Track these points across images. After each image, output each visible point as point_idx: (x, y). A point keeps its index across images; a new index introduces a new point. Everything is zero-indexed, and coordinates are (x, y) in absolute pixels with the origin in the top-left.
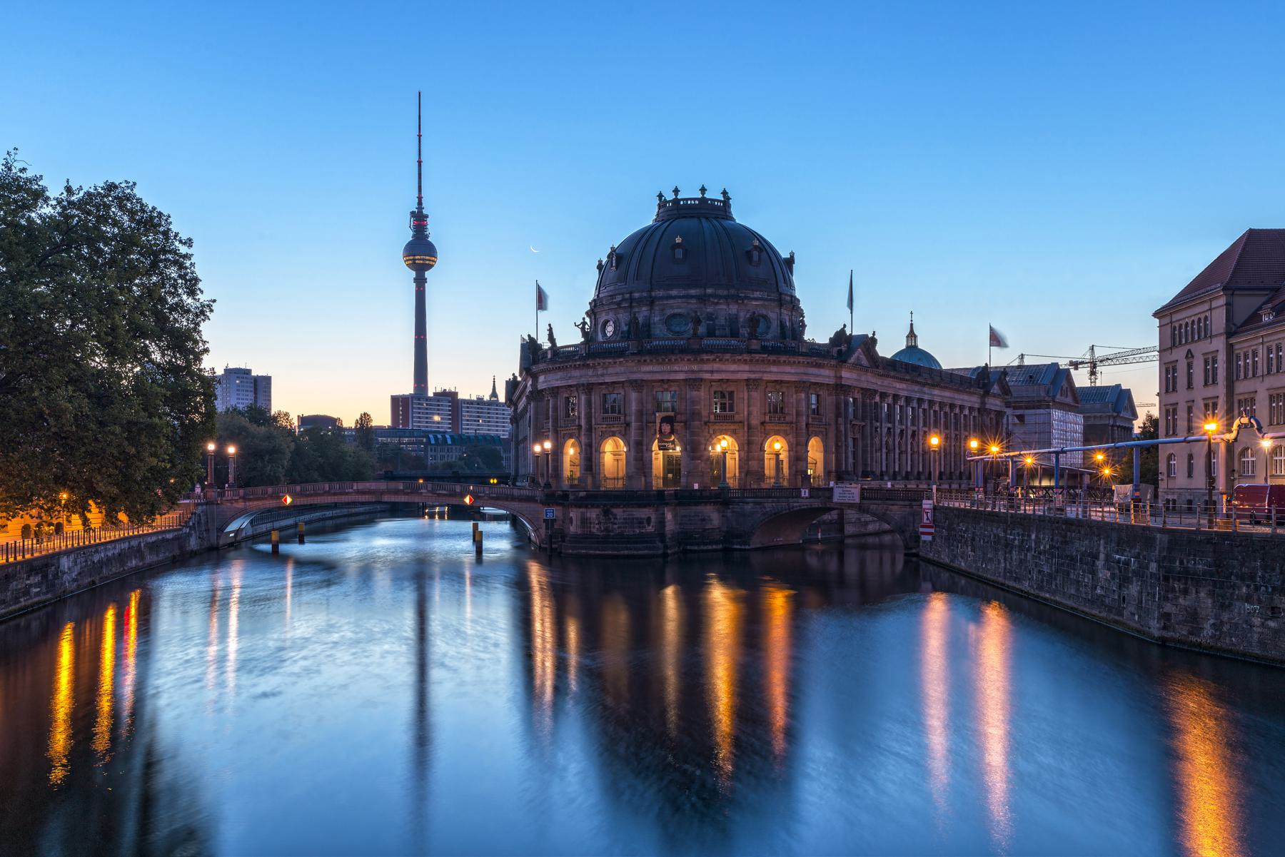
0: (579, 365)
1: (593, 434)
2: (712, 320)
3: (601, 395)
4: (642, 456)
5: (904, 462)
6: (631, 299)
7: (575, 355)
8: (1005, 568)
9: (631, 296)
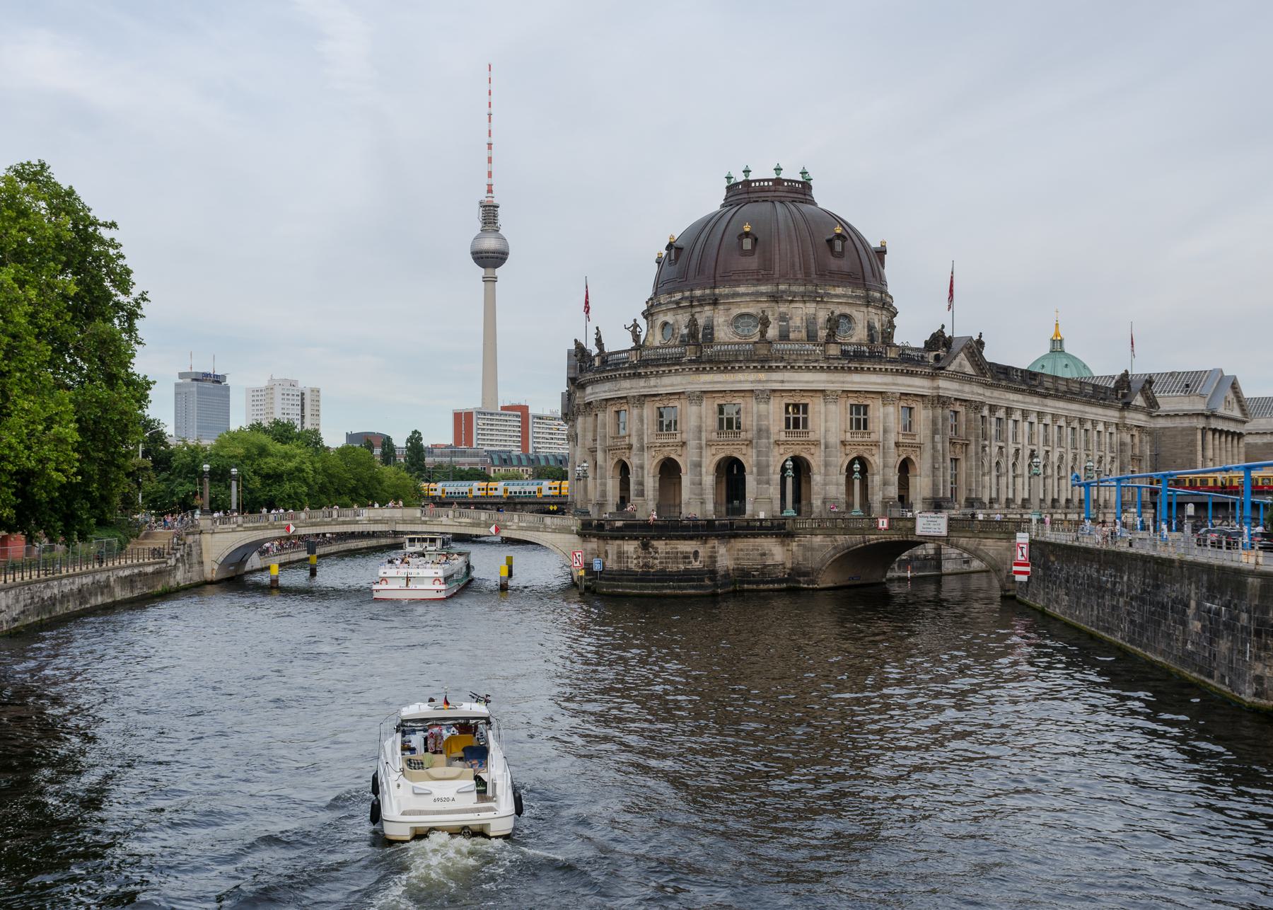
4: (701, 480)
7: (624, 363)
8: (1098, 617)
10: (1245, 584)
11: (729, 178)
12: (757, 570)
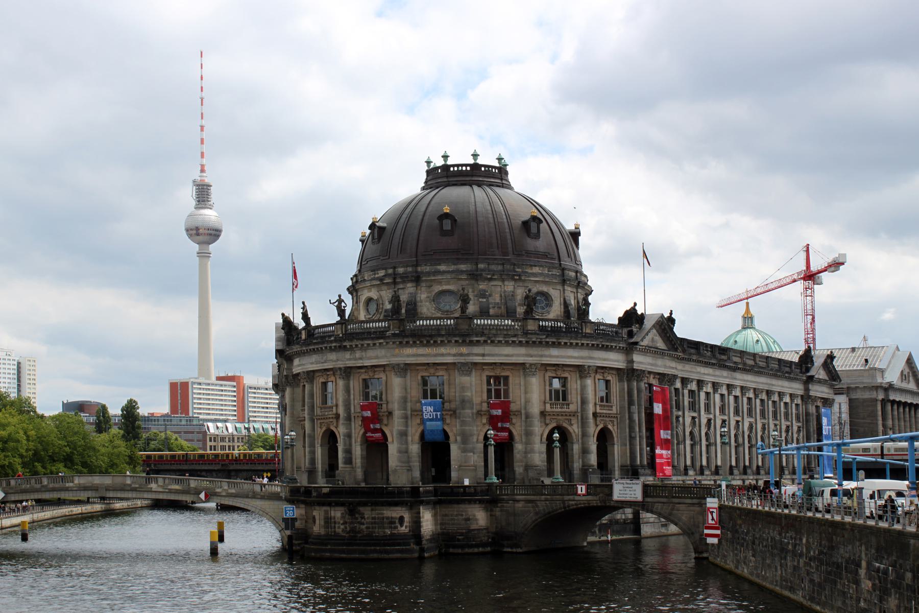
0: (335, 346)
1: (353, 423)
2: (485, 298)
3: (361, 381)
5: (713, 455)
6: (395, 274)
7: (330, 336)
8: (781, 576)
9: (394, 271)
10: (908, 545)
11: (428, 163)
12: (462, 534)
